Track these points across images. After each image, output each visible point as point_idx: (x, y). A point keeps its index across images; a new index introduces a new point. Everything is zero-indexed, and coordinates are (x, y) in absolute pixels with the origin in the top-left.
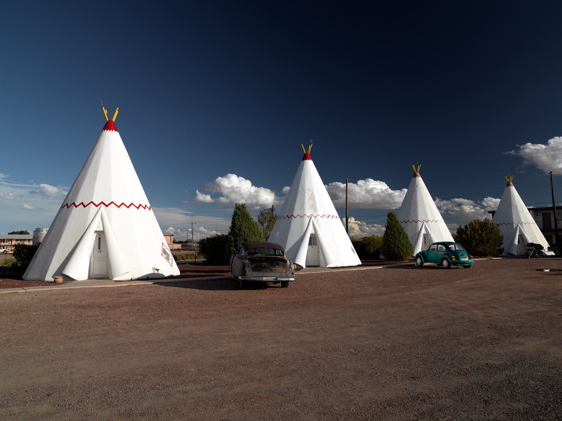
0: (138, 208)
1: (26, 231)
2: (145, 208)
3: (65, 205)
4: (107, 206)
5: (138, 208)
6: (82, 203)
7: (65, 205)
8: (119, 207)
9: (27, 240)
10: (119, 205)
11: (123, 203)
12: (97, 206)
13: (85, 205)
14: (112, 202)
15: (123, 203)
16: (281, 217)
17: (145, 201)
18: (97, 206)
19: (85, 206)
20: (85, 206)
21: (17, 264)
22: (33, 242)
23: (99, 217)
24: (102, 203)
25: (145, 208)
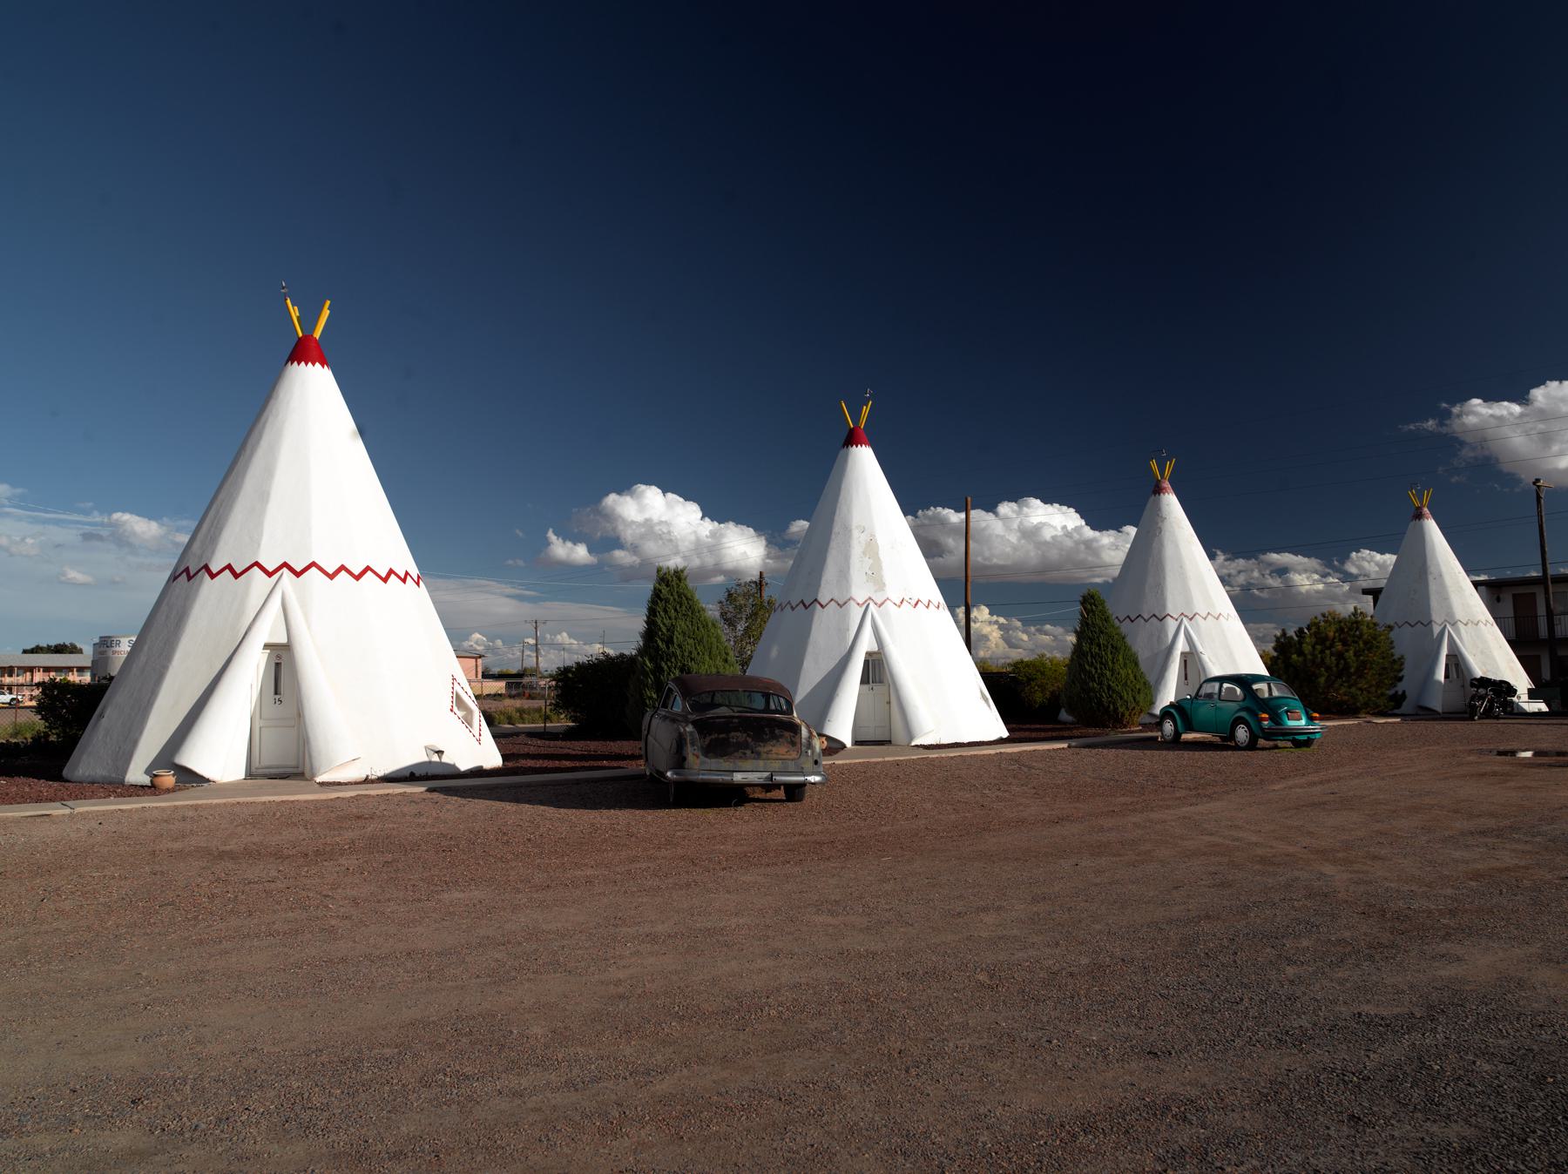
0: (385, 580)
2: (404, 581)
3: (182, 572)
4: (298, 574)
5: (385, 580)
6: (229, 567)
7: (182, 572)
8: (331, 576)
12: (270, 574)
17: (405, 561)
18: (270, 574)
19: (236, 576)
20: (236, 576)
22: (93, 676)
23: (275, 605)
24: (285, 565)
25: (404, 581)
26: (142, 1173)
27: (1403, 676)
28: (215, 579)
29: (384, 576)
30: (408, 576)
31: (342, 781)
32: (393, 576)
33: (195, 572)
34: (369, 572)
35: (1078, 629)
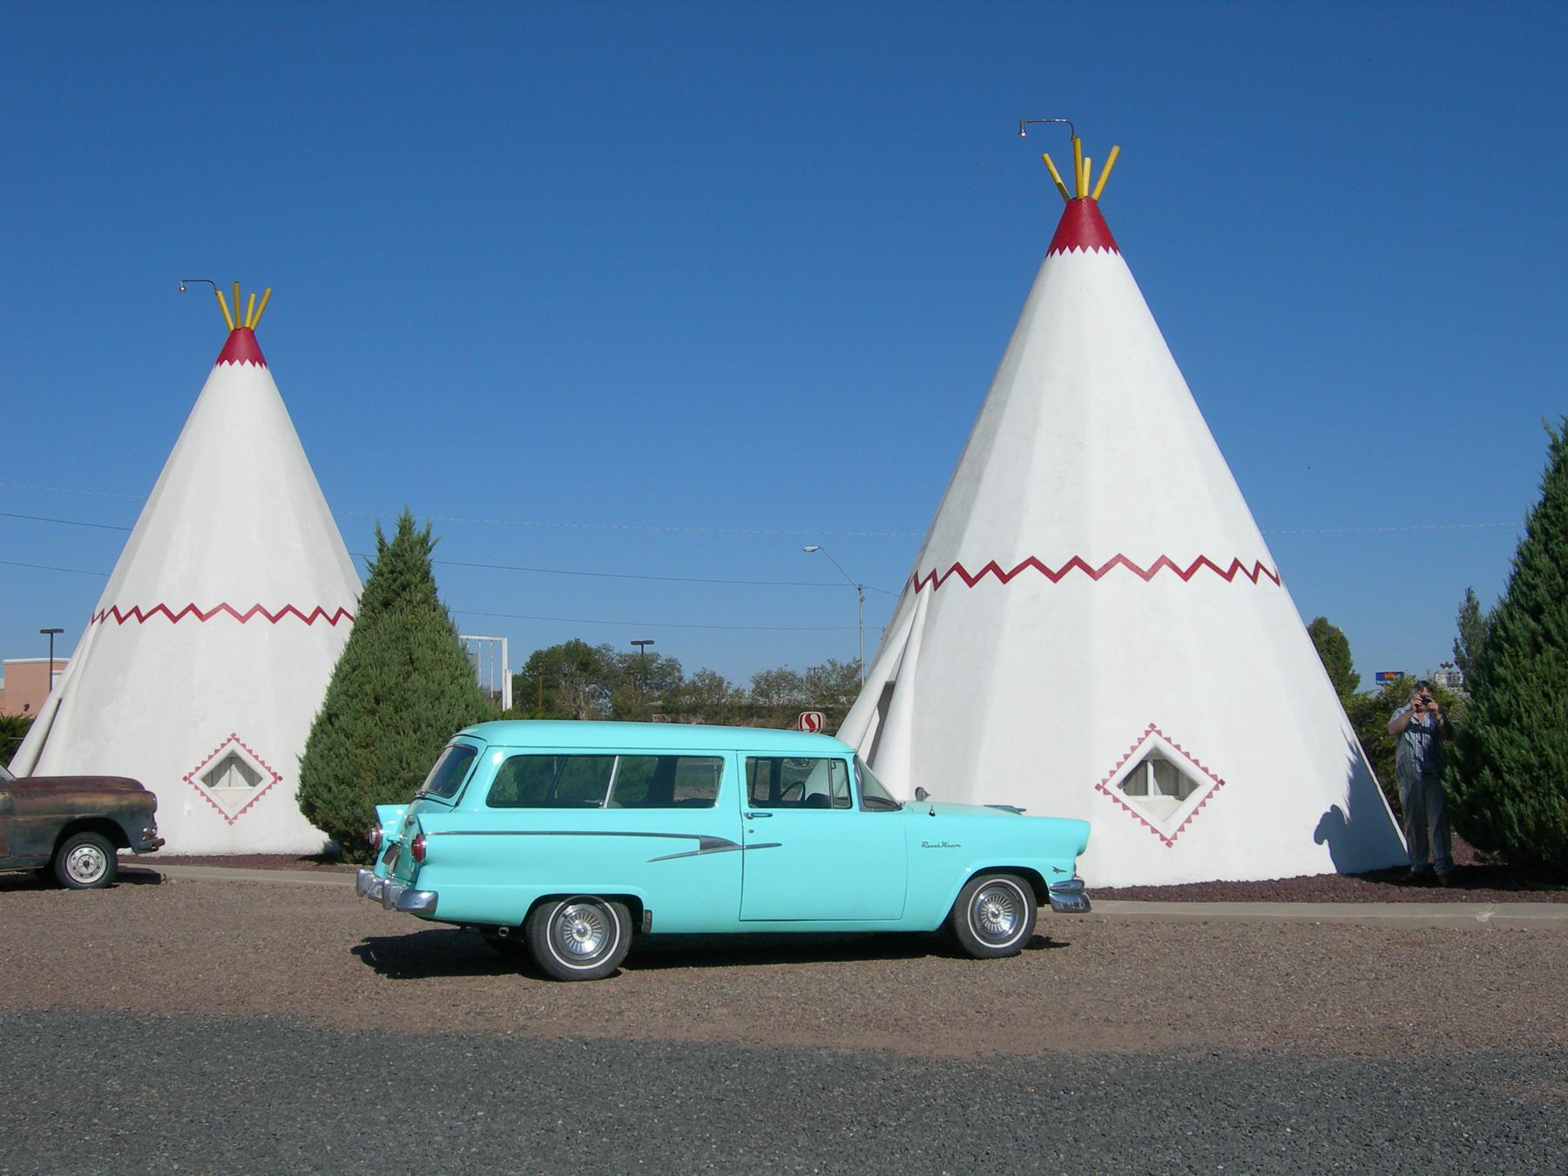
1: (584, 643)
3: (109, 613)
5: (1229, 576)
6: (993, 566)
7: (109, 613)
8: (1147, 576)
9: (508, 702)
10: (273, 615)
11: (243, 622)
13: (191, 613)
14: (1120, 558)
15: (243, 622)
16: (930, 583)
17: (1254, 550)
19: (1005, 578)
20: (1005, 578)
21: (377, 831)
25: (1254, 578)
26: (96, 1172)
27: (828, 661)
28: (278, 622)
29: (1226, 570)
30: (1261, 571)
31: (190, 853)
32: (343, 615)
33: (132, 616)
34: (1203, 566)
35: (1485, 611)
